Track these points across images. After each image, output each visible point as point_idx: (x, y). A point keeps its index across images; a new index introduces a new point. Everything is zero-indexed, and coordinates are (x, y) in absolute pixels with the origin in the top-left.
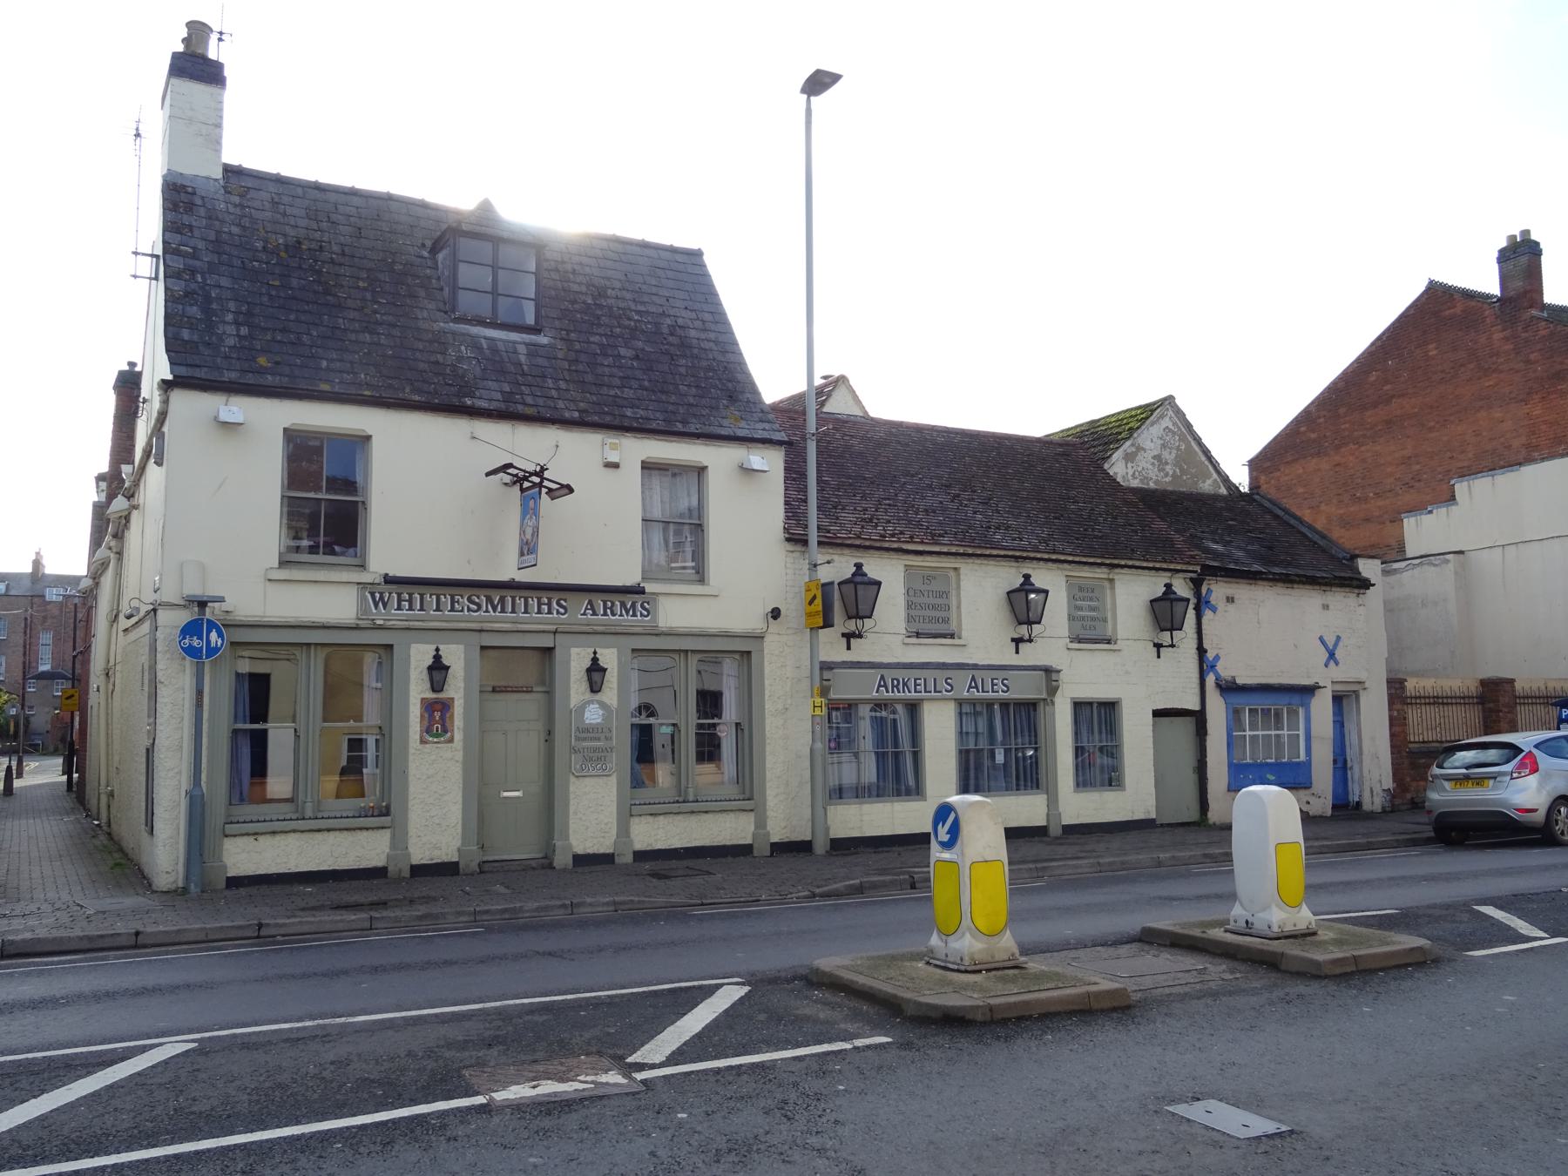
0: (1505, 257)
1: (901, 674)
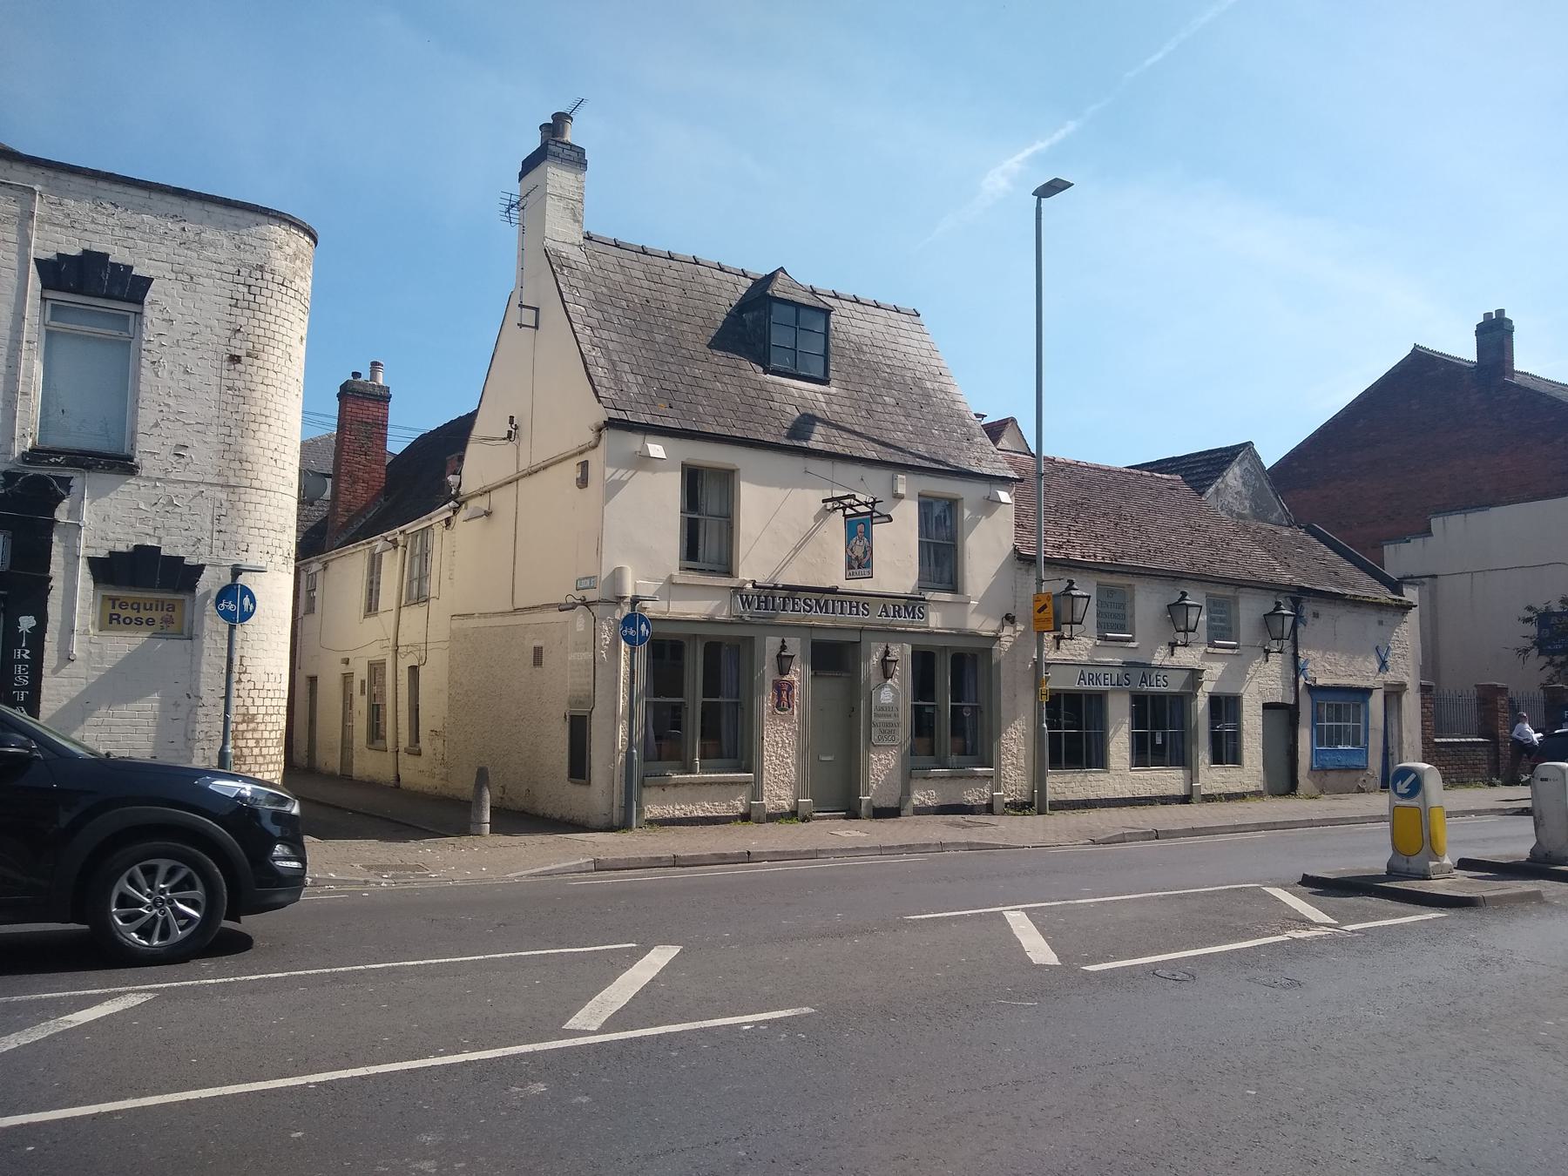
0: (1482, 331)
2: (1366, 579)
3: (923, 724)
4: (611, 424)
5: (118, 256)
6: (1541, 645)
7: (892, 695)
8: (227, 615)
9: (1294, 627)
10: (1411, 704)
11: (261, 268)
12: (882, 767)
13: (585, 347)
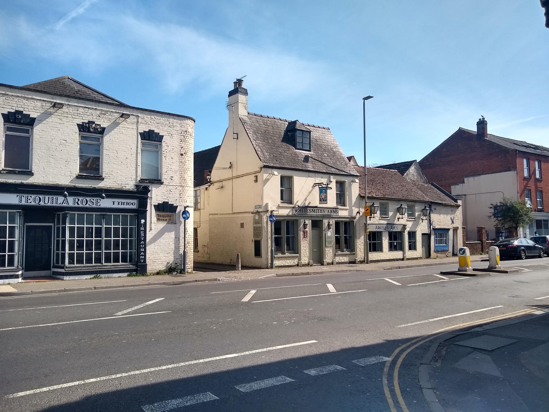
1: (379, 226)
2: (448, 198)
3: (338, 241)
4: (265, 167)
5: (156, 131)
6: (495, 215)
7: (330, 234)
8: (184, 218)
9: (430, 213)
10: (460, 232)
11: (186, 131)
12: (329, 253)
13: (255, 146)
